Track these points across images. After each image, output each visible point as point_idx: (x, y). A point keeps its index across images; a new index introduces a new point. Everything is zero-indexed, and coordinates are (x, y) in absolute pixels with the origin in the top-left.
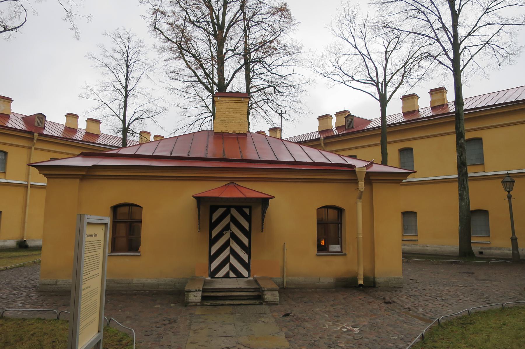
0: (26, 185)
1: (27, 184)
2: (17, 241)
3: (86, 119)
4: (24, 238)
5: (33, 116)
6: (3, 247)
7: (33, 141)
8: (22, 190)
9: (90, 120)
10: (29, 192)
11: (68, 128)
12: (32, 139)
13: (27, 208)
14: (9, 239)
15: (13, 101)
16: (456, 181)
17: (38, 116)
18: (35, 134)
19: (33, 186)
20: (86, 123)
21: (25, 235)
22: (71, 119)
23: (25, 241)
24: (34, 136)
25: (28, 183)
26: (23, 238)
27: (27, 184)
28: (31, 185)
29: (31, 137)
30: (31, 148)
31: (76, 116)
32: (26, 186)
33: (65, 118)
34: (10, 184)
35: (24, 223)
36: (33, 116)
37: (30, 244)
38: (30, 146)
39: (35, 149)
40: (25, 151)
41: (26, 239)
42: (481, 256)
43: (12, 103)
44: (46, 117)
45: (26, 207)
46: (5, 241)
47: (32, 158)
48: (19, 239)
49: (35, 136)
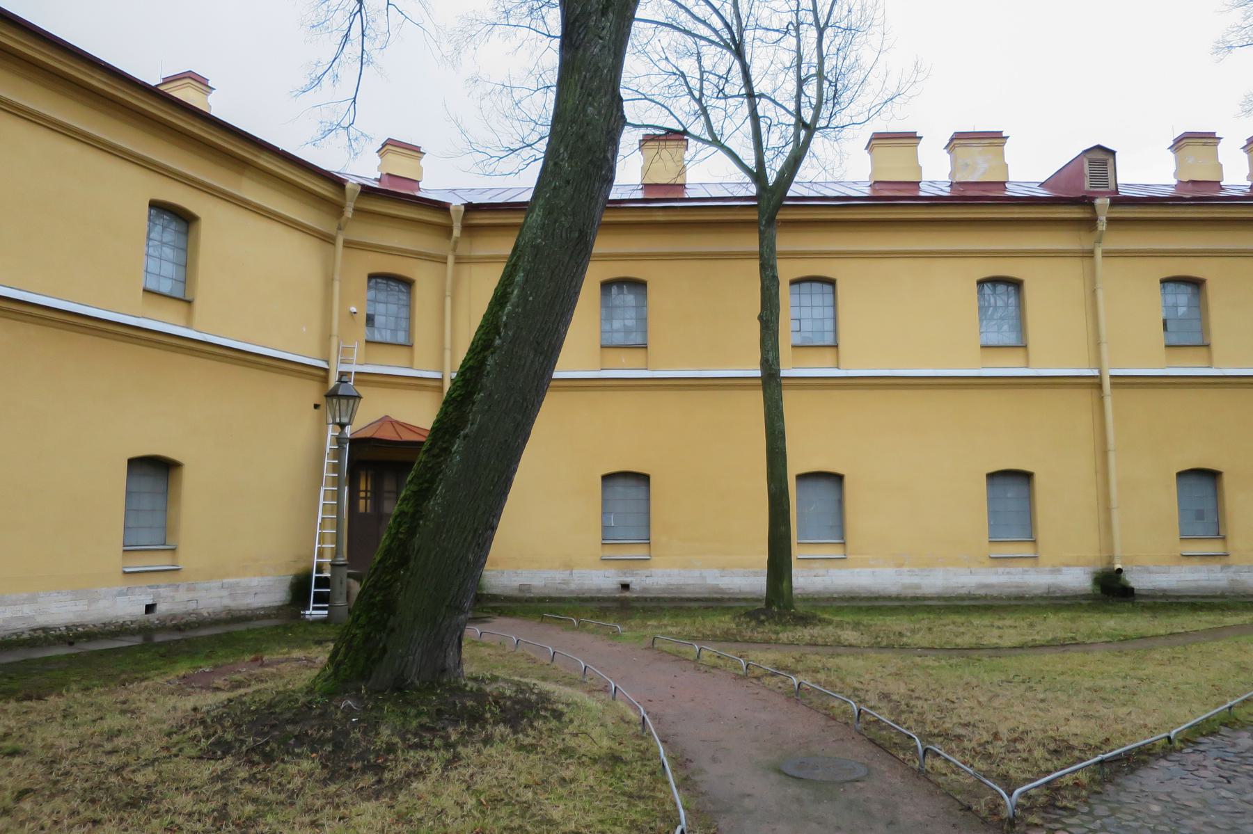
0: (1097, 381)
1: (1100, 377)
2: (1095, 573)
3: (1245, 143)
4: (1116, 560)
5: (1072, 164)
6: (1054, 592)
7: (1097, 228)
8: (1084, 397)
9: (960, 139)
10: (1108, 402)
11: (1190, 184)
12: (1091, 223)
13: (1112, 458)
14: (1067, 565)
15: (1007, 137)
16: (758, 385)
17: (1091, 155)
18: (1098, 201)
19: (1121, 382)
20: (1246, 156)
21: (1118, 551)
22: (1194, 151)
23: (1120, 571)
24: (1095, 211)
25: (1100, 372)
26: (1111, 560)
27: (441, 380)
28: (1112, 377)
29: (1088, 215)
30: (1090, 254)
31: (1209, 139)
32: (1095, 383)
33: (1171, 156)
34: (248, 357)
35: (1108, 509)
36: (1072, 164)
37: (1137, 580)
38: (1088, 247)
39: (1108, 254)
40: (1074, 268)
41: (1121, 564)
42: (627, 594)
43: (1005, 147)
44: (1117, 154)
45: (1105, 453)
46: (1055, 570)
47: (1099, 285)
48: (1100, 566)
49: (1098, 209)
